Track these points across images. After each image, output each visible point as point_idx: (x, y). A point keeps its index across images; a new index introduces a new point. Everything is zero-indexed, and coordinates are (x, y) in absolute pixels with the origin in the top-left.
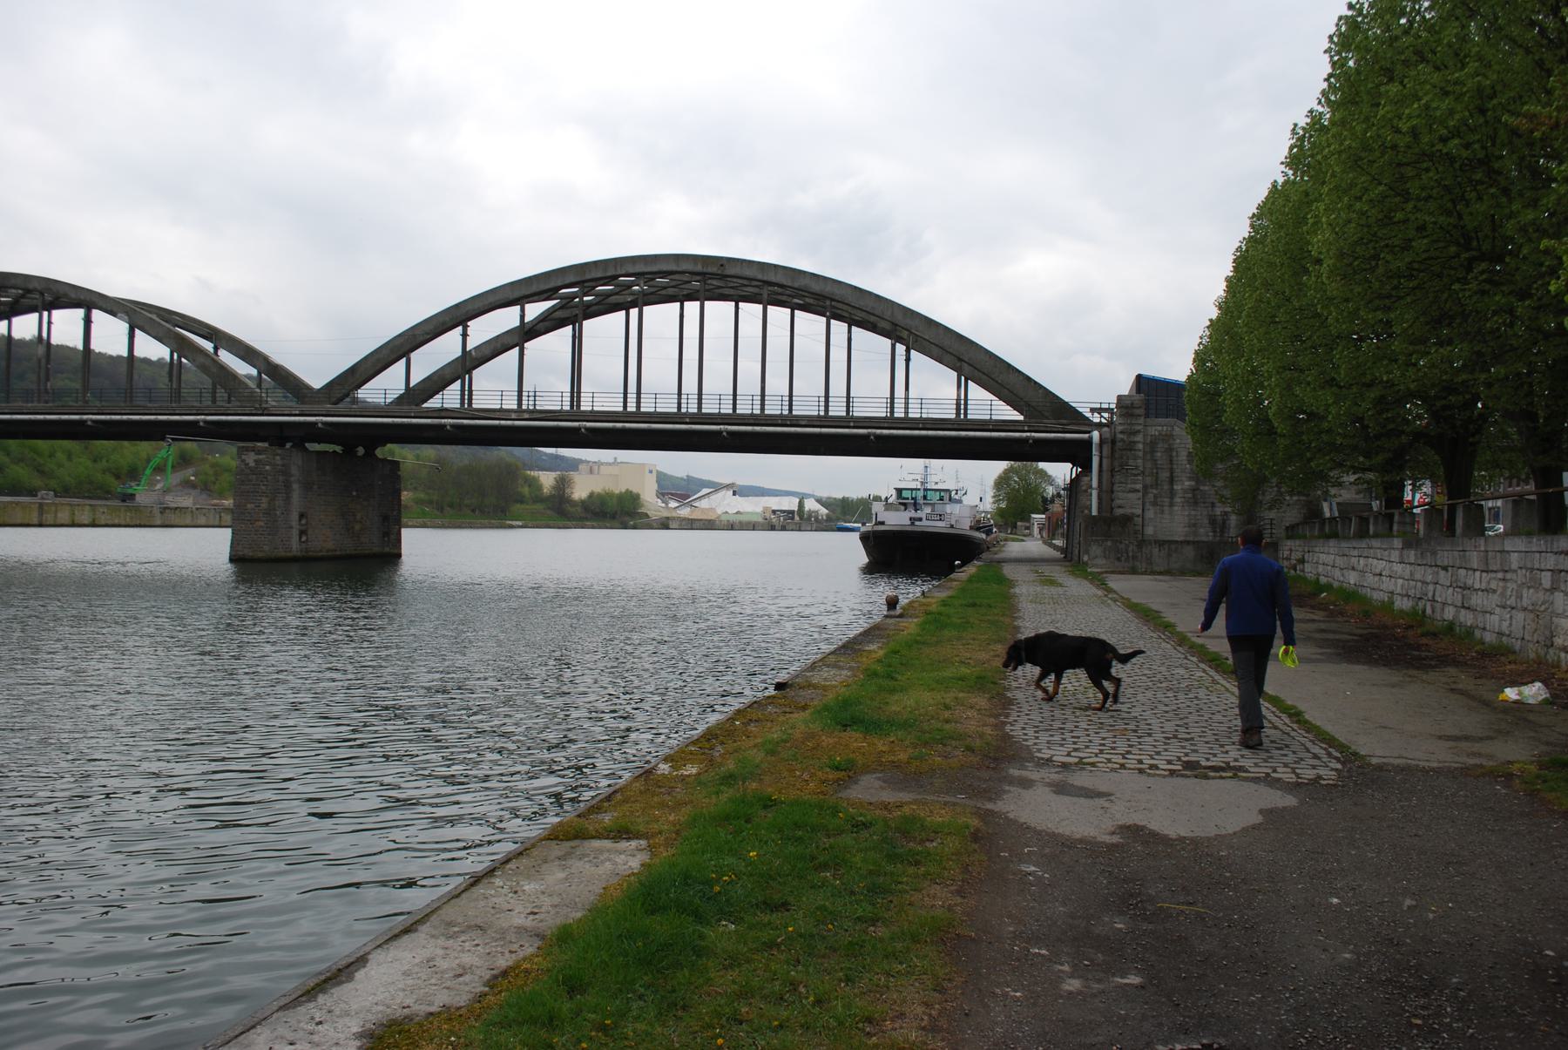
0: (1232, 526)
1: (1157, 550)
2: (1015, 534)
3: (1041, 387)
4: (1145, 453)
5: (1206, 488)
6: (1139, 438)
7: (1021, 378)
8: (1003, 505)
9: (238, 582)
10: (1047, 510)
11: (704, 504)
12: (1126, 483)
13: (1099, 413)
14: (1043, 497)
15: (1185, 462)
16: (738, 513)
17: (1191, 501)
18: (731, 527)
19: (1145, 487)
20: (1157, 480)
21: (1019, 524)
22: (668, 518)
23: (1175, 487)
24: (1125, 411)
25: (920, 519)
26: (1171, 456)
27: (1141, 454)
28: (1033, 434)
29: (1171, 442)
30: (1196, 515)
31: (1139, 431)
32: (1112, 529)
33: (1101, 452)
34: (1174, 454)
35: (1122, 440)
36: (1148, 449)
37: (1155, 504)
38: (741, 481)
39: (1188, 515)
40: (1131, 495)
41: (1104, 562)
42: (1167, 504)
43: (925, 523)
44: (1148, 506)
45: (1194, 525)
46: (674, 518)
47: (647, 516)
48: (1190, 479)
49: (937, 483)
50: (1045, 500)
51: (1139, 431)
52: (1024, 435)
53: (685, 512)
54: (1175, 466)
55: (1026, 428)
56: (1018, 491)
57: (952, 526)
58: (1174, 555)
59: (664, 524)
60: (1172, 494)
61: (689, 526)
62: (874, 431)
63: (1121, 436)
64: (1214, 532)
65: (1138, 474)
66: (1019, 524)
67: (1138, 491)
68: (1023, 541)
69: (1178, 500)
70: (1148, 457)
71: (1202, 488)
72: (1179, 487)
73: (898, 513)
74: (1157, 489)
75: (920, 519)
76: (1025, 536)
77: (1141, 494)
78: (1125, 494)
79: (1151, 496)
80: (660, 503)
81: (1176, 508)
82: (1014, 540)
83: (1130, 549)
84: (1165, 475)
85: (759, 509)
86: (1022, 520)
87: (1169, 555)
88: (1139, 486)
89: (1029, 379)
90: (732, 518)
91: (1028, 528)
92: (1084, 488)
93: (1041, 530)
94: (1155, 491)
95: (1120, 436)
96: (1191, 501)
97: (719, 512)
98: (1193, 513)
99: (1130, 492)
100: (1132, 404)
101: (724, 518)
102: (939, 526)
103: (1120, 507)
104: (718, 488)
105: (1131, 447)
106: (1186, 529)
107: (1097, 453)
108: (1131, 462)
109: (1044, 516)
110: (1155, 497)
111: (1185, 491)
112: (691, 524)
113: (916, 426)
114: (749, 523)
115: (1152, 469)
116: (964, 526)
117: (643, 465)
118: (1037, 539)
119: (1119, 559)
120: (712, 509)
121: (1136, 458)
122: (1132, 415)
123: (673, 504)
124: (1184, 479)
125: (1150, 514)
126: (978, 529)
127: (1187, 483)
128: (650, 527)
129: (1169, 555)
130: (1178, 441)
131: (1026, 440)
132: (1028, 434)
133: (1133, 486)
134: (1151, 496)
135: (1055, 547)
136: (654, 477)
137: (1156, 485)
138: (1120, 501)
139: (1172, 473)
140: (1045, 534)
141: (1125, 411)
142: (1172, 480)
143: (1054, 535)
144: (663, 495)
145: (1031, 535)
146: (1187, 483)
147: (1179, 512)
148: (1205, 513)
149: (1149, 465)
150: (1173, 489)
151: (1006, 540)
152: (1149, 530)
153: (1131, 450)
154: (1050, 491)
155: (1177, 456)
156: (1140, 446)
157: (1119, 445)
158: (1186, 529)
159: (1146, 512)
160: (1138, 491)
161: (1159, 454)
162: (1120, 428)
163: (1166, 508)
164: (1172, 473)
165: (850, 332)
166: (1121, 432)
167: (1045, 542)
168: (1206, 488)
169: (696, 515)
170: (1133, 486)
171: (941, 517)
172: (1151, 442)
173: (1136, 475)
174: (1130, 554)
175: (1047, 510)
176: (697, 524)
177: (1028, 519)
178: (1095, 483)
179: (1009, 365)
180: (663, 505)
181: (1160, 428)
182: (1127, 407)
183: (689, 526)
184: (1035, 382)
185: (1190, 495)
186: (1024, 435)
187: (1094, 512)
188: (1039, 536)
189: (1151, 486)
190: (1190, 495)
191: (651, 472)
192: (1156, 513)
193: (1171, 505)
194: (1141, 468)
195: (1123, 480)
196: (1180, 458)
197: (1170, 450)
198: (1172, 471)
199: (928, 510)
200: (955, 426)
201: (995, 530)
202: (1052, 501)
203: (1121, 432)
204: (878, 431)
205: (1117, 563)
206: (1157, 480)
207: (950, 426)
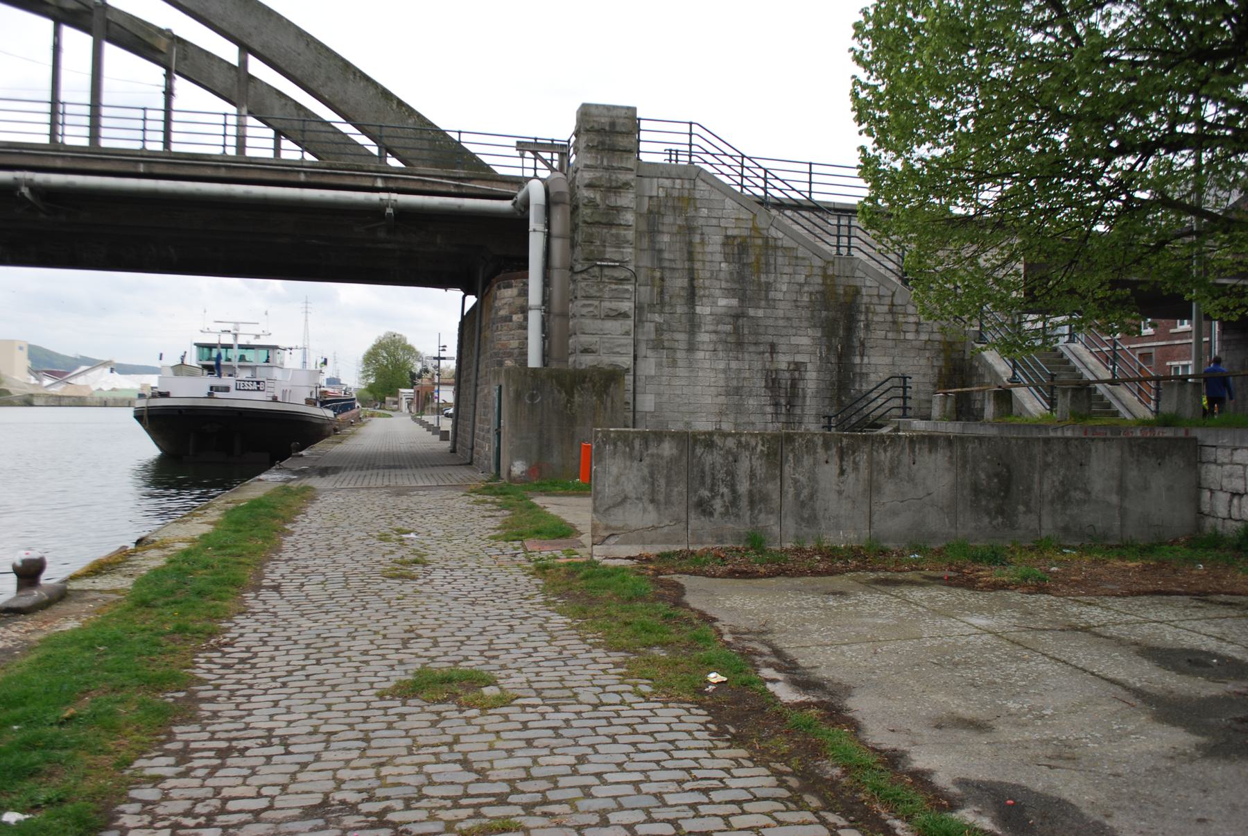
0: (809, 392)
1: (833, 468)
2: (384, 409)
3: (411, 112)
4: (639, 234)
5: (760, 313)
6: (626, 199)
7: (372, 91)
8: (372, 380)
9: (935, 385)
10: (415, 384)
11: (80, 381)
12: (601, 299)
13: (534, 152)
14: (411, 372)
15: (719, 257)
16: (114, 389)
17: (731, 339)
18: (105, 404)
19: (639, 308)
20: (662, 292)
21: (387, 398)
22: (32, 395)
23: (698, 309)
24: (596, 139)
25: (227, 389)
26: (690, 243)
27: (630, 235)
28: (394, 196)
29: (691, 213)
30: (739, 370)
31: (626, 185)
32: (577, 399)
33: (548, 225)
34: (697, 239)
35: (591, 203)
36: (643, 227)
37: (657, 345)
38: (118, 360)
39: (724, 371)
40: (610, 325)
41: (651, 517)
42: (683, 345)
43: (233, 394)
44: (643, 350)
45: (737, 391)
46: (38, 396)
47: (7, 392)
48: (730, 293)
49: (258, 336)
50: (413, 376)
51: (626, 185)
52: (375, 197)
53: (58, 390)
54: (698, 265)
55: (379, 183)
56: (387, 366)
57: (275, 399)
58: (889, 487)
59: (28, 402)
60: (693, 325)
61: (57, 403)
62: (28, 175)
63: (586, 193)
64: (776, 405)
65: (626, 279)
66: (387, 398)
67: (624, 315)
68: (390, 416)
69: (703, 337)
70: (645, 243)
71: (751, 312)
72: (707, 310)
73: (192, 379)
74: (661, 312)
75: (227, 389)
76: (393, 411)
77: (630, 323)
78: (598, 324)
79: (649, 328)
80: (33, 380)
81: (700, 355)
82: (380, 416)
83: (744, 466)
84: (678, 283)
85: (137, 387)
86: (391, 395)
87: (872, 488)
88: (627, 306)
89: (386, 95)
90: (105, 396)
91: (396, 403)
92: (502, 313)
93: (409, 405)
94: (657, 318)
95: (586, 193)
96: (731, 339)
97: (94, 388)
98: (734, 365)
99: (608, 317)
100: (613, 124)
101: (97, 395)
102: (255, 400)
103: (586, 351)
104: (94, 364)
105: (609, 220)
106: (722, 399)
107: (541, 227)
108: (610, 252)
109: (412, 391)
110: (659, 330)
111: (718, 319)
112: (58, 401)
113: (130, 168)
114: (123, 400)
115: (653, 270)
116: (297, 402)
117: (12, 342)
118: (405, 415)
119: (703, 507)
120: (87, 387)
121: (619, 243)
122: (613, 150)
123: (47, 381)
124: (718, 292)
125: (648, 366)
126: (324, 404)
127: (722, 302)
128: (10, 404)
129: (872, 488)
130: (704, 212)
131: (376, 211)
132: (384, 196)
133: (614, 305)
134: (649, 328)
135: (434, 430)
136: (24, 354)
137: (661, 303)
138: (585, 339)
139: (692, 280)
140: (413, 409)
141: (596, 139)
142: (692, 296)
143: (423, 410)
144: (37, 372)
145: (398, 409)
146: (722, 302)
147: (707, 365)
148: (758, 365)
149: (646, 261)
150: (694, 313)
151: (372, 416)
152: (647, 402)
153: (610, 225)
154: (418, 367)
155: (703, 242)
156: (629, 217)
157: (585, 212)
158: (722, 399)
159: (641, 364)
160: (624, 315)
161: (666, 238)
162: (587, 176)
163: (681, 355)
164: (692, 280)
165: (57, 34)
166: (590, 186)
167: (414, 419)
168: (760, 313)
169: (69, 392)
170: (614, 305)
171: (259, 385)
172: (650, 212)
173: (621, 281)
174: (743, 487)
175: (415, 384)
176: (66, 401)
177: (396, 394)
178: (535, 296)
179: (347, 65)
180: (37, 382)
181: (667, 183)
182: (600, 131)
183: (57, 403)
184: (400, 103)
185: (729, 328)
186: (375, 197)
187: (534, 361)
188: (407, 411)
189: (651, 305)
190: (729, 328)
191: (21, 348)
192: (659, 365)
193: (692, 348)
194: (632, 267)
195: (593, 292)
196: (709, 249)
197: (689, 229)
198: (692, 275)
199: (244, 375)
200: (223, 173)
201: (357, 404)
202: (420, 376)
203: (590, 186)
204: (40, 177)
205: (696, 522)
206: (662, 292)
207: (209, 172)
